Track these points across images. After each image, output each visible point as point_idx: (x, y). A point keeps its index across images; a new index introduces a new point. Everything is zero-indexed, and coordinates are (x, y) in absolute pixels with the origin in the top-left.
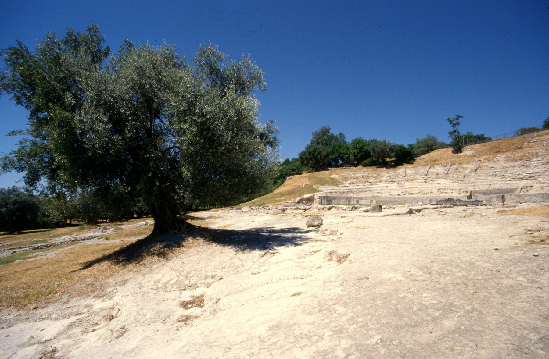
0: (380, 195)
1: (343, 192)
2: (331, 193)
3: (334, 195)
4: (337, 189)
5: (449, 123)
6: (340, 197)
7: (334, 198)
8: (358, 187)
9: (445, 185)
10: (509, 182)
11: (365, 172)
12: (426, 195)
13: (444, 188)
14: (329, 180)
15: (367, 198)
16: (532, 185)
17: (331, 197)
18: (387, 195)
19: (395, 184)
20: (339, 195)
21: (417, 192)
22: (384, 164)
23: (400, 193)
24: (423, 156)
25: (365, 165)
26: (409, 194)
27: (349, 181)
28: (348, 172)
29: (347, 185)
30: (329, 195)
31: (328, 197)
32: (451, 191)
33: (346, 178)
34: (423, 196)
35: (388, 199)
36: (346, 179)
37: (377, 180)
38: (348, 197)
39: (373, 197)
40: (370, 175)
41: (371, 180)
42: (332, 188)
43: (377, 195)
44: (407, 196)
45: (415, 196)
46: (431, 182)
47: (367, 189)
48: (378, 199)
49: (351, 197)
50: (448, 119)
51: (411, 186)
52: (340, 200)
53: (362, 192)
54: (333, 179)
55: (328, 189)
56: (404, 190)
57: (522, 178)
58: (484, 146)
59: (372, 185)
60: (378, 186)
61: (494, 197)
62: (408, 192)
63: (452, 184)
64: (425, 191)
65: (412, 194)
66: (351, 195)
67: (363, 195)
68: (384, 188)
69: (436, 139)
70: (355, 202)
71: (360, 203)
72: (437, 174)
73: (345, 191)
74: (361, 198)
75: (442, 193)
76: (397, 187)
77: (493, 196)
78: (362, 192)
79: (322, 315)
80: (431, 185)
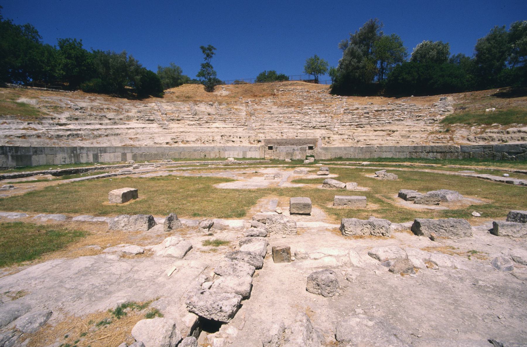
0: (137, 144)
1: (58, 136)
2: (24, 136)
3: (35, 143)
4: (41, 129)
5: (201, 51)
6: (52, 149)
7: (37, 151)
8: (89, 127)
9: (225, 130)
10: (300, 131)
11: (92, 101)
12: (207, 145)
13: (228, 134)
14: (15, 107)
15: (115, 149)
16: (328, 135)
17: (27, 149)
18: (150, 143)
19: (155, 125)
20: (50, 143)
21: (194, 139)
22: (122, 93)
23: (169, 140)
24: (172, 90)
25: (89, 90)
26: (182, 142)
27: (67, 114)
28: (59, 97)
29: (63, 121)
30: (19, 143)
31: (17, 148)
32: (239, 139)
33: (56, 107)
34: (203, 145)
35: (154, 152)
36: (57, 109)
37: (121, 117)
38: (74, 149)
39: (125, 147)
40: (106, 106)
41: (111, 115)
42: (25, 125)
43: (132, 142)
44: (182, 145)
45: (192, 145)
46: (207, 125)
47: (108, 132)
48: (136, 151)
49: (82, 148)
50: (202, 48)
51: (181, 130)
52: (55, 155)
53: (100, 136)
54: (23, 104)
55: (14, 126)
56: (174, 136)
57: (314, 128)
58: (237, 87)
59: (115, 123)
60: (128, 126)
61: (297, 150)
62: (181, 138)
63: (235, 130)
64: (205, 138)
65: (187, 141)
66: (77, 143)
67: (104, 143)
68: (140, 131)
69: (181, 72)
70: (91, 159)
71: (101, 160)
72: (209, 114)
73: (61, 133)
74: (104, 150)
75: (227, 141)
76: (161, 130)
77: (295, 147)
78: (100, 136)
79: (9, 217)
80: (208, 130)
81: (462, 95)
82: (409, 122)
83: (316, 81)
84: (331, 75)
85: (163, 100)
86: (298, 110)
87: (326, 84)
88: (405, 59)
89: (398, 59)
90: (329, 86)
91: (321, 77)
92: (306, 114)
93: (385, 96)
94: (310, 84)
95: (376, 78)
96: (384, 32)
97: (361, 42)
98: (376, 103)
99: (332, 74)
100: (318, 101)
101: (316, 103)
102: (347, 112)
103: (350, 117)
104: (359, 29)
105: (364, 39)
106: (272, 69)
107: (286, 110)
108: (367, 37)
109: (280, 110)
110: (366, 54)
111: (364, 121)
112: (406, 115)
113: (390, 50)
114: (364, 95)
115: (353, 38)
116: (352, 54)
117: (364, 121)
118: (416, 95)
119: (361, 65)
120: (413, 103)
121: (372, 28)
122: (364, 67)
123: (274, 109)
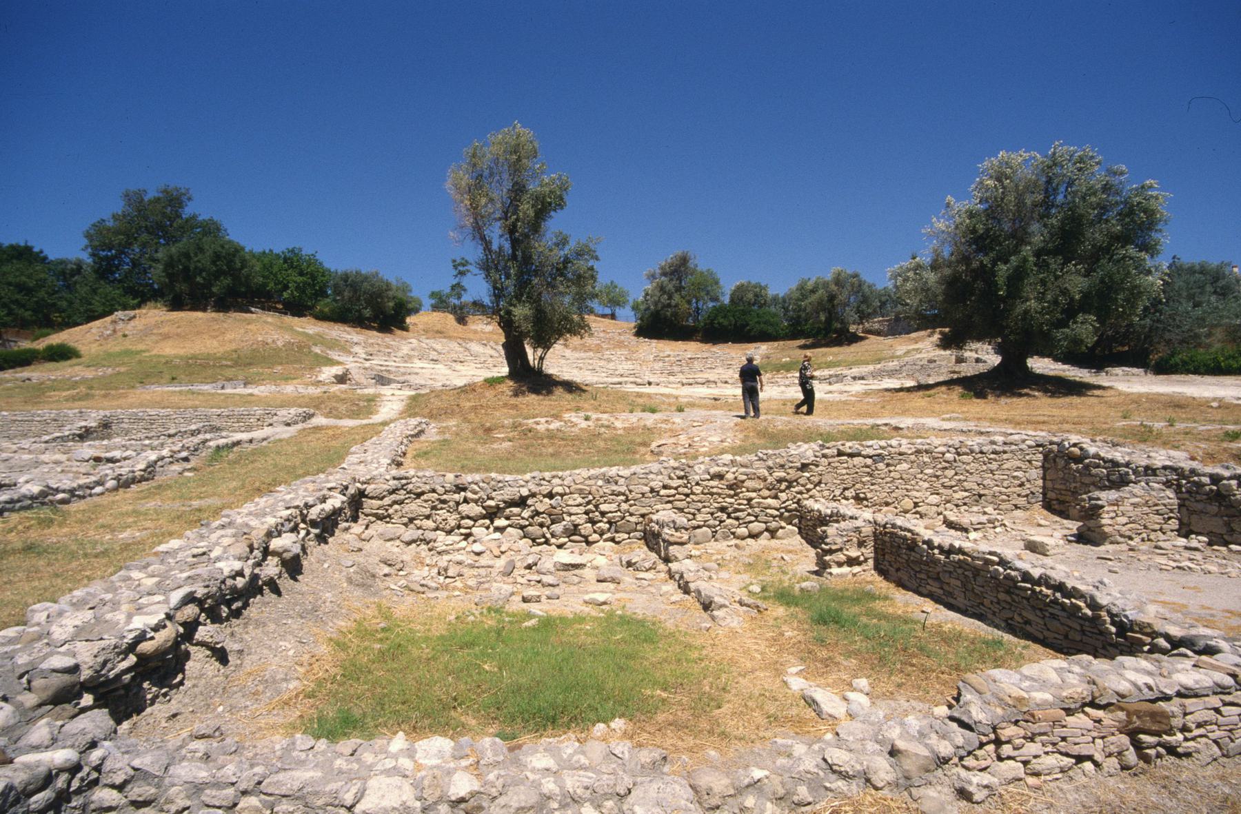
50: (454, 261)
81: (776, 344)
82: (720, 370)
83: (613, 316)
84: (633, 308)
85: (410, 334)
86: (599, 355)
87: (627, 320)
88: (722, 298)
89: (715, 299)
90: (633, 324)
91: (618, 311)
92: (609, 361)
93: (702, 341)
94: (607, 321)
95: (690, 320)
96: (702, 263)
97: (672, 273)
98: (691, 349)
99: (635, 308)
100: (620, 345)
101: (620, 347)
102: (657, 359)
103: (661, 364)
104: (667, 257)
105: (676, 271)
106: (176, 182)
107: (583, 355)
108: (679, 269)
109: (577, 355)
110: (679, 289)
111: (676, 369)
112: (719, 363)
113: (707, 286)
114: (676, 339)
115: (662, 268)
116: (662, 289)
117: (676, 369)
118: (733, 342)
119: (673, 303)
120: (727, 351)
121: (684, 260)
122: (676, 306)
123: (568, 353)
